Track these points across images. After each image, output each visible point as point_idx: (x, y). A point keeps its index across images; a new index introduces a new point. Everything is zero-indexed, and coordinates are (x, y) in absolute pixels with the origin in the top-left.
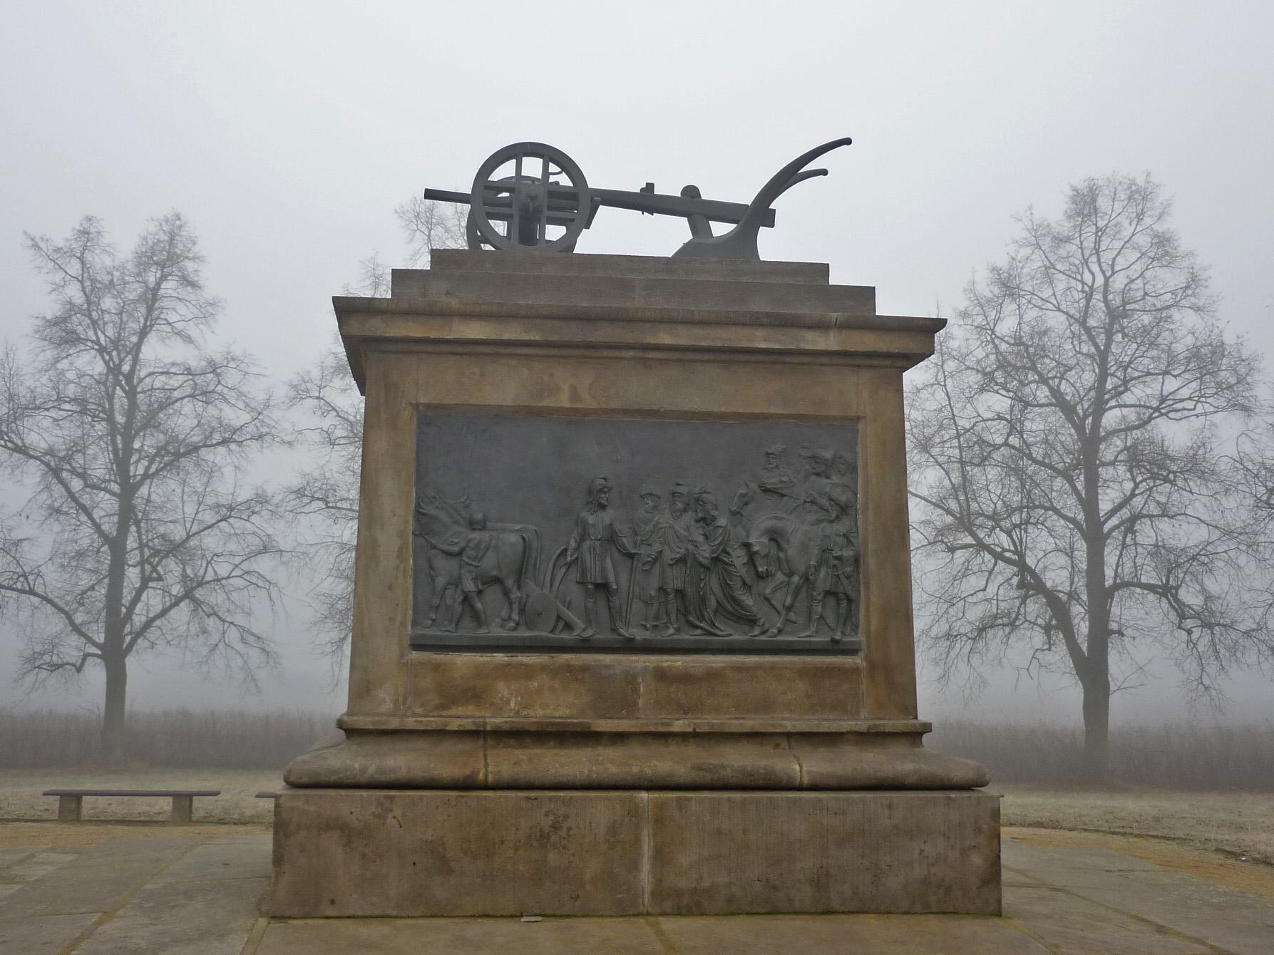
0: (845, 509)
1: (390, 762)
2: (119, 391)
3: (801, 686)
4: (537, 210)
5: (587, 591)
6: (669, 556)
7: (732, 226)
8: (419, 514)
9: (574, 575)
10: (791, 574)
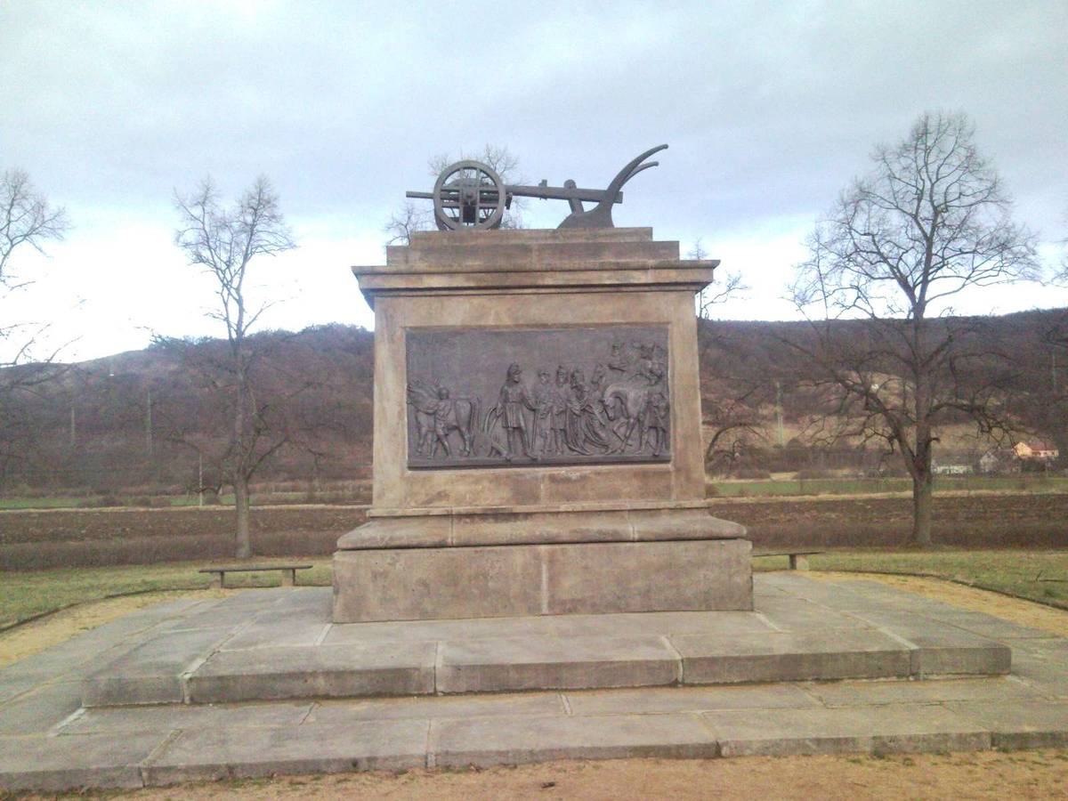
0: (661, 377)
1: (398, 533)
3: (636, 483)
4: (474, 203)
5: (508, 431)
6: (555, 410)
9: (500, 423)
10: (628, 418)
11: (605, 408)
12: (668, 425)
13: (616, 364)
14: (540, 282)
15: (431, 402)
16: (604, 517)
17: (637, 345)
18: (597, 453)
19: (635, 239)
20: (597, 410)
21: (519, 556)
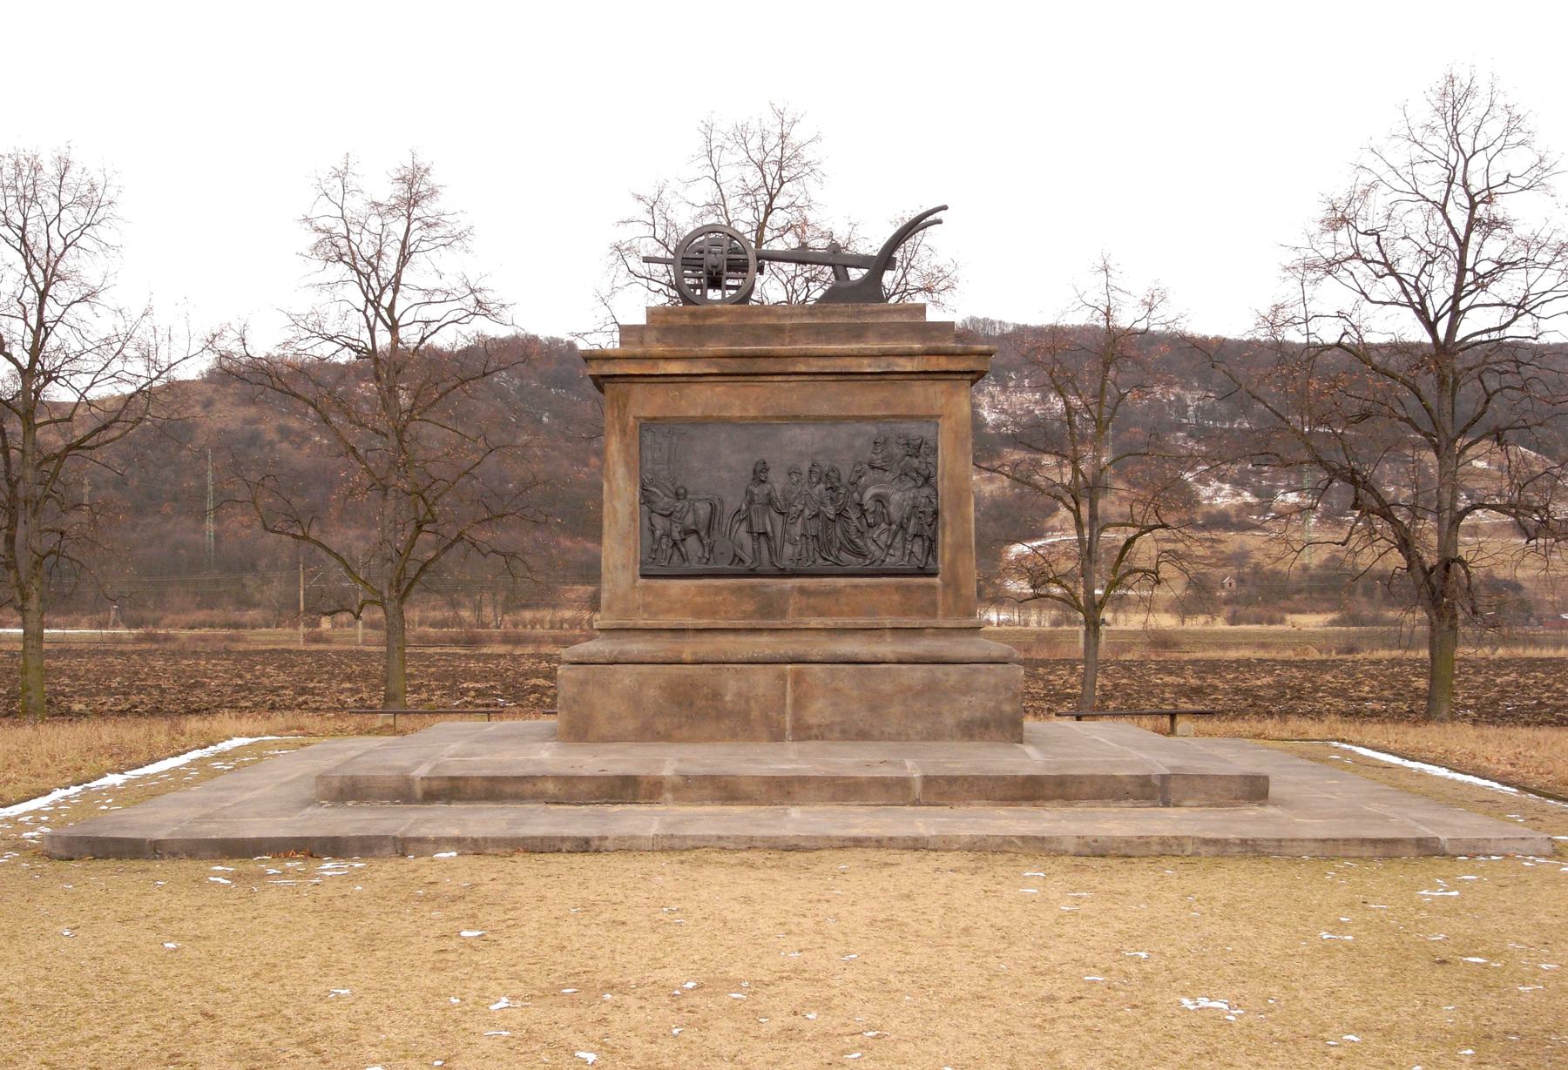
1: (628, 647)
2: (379, 323)
3: (896, 597)
4: (719, 273)
7: (865, 271)
8: (644, 489)
9: (744, 527)
11: (863, 512)
12: (935, 533)
13: (878, 463)
14: (791, 369)
15: (663, 502)
16: (860, 637)
17: (902, 441)
18: (854, 562)
19: (905, 319)
20: (853, 515)
21: (762, 677)
